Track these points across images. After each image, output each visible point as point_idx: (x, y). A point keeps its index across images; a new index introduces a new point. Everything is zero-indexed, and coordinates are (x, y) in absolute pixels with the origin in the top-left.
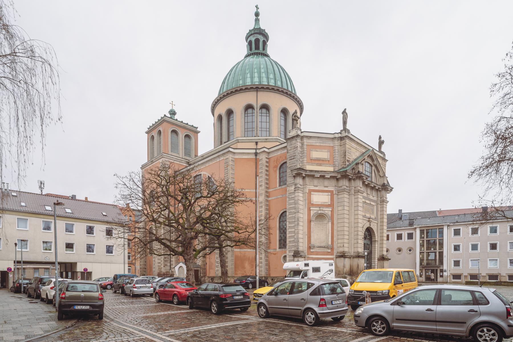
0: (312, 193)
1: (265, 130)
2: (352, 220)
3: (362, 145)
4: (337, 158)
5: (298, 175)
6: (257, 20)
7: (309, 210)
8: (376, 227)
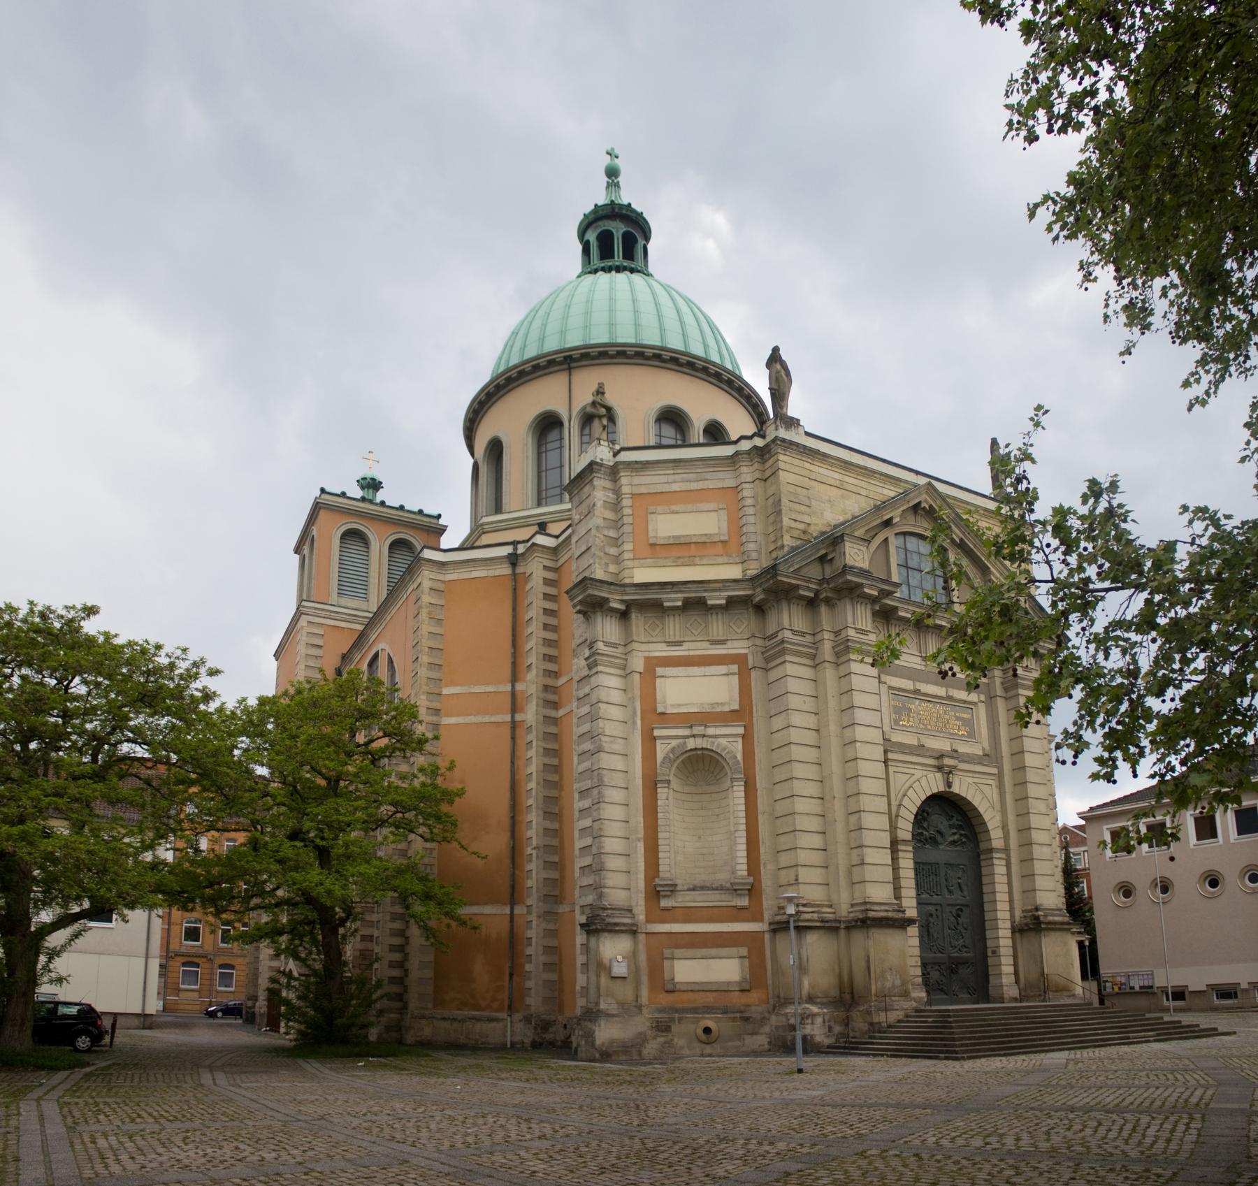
0: (659, 671)
2: (835, 766)
3: (871, 473)
4: (751, 529)
5: (592, 607)
7: (650, 740)
8: (992, 792)
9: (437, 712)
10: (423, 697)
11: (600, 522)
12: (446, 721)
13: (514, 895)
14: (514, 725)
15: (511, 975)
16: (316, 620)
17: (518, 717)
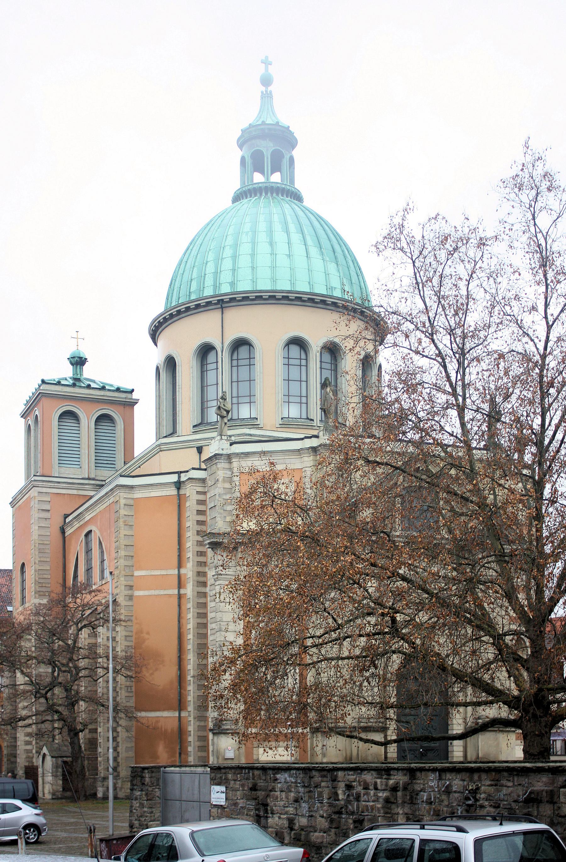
1: (298, 400)
6: (267, 97)
9: (131, 587)
10: (122, 579)
11: (221, 491)
12: (137, 593)
13: (181, 705)
14: (180, 597)
15: (180, 754)
16: (44, 490)
17: (182, 591)
